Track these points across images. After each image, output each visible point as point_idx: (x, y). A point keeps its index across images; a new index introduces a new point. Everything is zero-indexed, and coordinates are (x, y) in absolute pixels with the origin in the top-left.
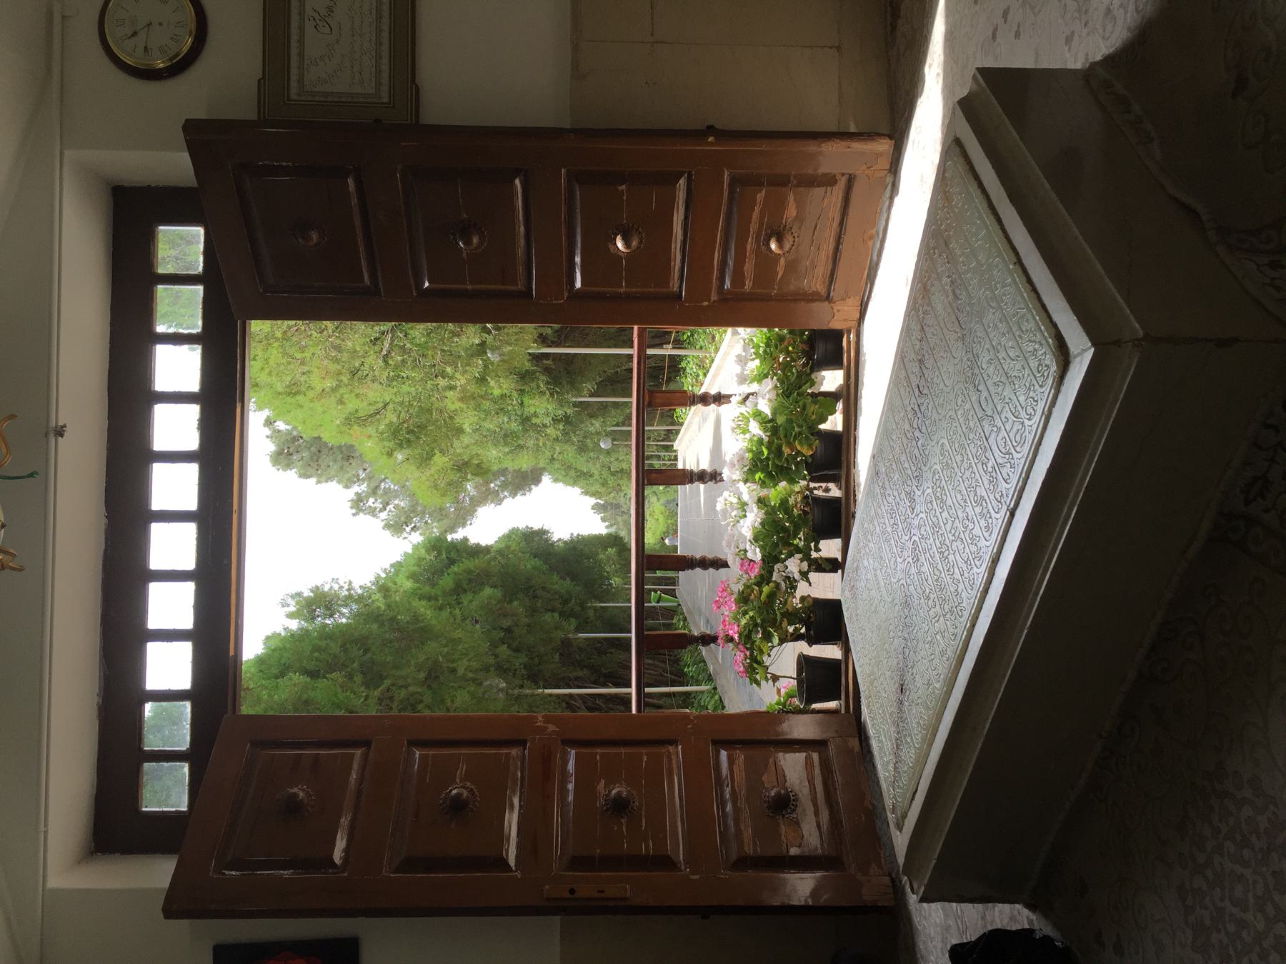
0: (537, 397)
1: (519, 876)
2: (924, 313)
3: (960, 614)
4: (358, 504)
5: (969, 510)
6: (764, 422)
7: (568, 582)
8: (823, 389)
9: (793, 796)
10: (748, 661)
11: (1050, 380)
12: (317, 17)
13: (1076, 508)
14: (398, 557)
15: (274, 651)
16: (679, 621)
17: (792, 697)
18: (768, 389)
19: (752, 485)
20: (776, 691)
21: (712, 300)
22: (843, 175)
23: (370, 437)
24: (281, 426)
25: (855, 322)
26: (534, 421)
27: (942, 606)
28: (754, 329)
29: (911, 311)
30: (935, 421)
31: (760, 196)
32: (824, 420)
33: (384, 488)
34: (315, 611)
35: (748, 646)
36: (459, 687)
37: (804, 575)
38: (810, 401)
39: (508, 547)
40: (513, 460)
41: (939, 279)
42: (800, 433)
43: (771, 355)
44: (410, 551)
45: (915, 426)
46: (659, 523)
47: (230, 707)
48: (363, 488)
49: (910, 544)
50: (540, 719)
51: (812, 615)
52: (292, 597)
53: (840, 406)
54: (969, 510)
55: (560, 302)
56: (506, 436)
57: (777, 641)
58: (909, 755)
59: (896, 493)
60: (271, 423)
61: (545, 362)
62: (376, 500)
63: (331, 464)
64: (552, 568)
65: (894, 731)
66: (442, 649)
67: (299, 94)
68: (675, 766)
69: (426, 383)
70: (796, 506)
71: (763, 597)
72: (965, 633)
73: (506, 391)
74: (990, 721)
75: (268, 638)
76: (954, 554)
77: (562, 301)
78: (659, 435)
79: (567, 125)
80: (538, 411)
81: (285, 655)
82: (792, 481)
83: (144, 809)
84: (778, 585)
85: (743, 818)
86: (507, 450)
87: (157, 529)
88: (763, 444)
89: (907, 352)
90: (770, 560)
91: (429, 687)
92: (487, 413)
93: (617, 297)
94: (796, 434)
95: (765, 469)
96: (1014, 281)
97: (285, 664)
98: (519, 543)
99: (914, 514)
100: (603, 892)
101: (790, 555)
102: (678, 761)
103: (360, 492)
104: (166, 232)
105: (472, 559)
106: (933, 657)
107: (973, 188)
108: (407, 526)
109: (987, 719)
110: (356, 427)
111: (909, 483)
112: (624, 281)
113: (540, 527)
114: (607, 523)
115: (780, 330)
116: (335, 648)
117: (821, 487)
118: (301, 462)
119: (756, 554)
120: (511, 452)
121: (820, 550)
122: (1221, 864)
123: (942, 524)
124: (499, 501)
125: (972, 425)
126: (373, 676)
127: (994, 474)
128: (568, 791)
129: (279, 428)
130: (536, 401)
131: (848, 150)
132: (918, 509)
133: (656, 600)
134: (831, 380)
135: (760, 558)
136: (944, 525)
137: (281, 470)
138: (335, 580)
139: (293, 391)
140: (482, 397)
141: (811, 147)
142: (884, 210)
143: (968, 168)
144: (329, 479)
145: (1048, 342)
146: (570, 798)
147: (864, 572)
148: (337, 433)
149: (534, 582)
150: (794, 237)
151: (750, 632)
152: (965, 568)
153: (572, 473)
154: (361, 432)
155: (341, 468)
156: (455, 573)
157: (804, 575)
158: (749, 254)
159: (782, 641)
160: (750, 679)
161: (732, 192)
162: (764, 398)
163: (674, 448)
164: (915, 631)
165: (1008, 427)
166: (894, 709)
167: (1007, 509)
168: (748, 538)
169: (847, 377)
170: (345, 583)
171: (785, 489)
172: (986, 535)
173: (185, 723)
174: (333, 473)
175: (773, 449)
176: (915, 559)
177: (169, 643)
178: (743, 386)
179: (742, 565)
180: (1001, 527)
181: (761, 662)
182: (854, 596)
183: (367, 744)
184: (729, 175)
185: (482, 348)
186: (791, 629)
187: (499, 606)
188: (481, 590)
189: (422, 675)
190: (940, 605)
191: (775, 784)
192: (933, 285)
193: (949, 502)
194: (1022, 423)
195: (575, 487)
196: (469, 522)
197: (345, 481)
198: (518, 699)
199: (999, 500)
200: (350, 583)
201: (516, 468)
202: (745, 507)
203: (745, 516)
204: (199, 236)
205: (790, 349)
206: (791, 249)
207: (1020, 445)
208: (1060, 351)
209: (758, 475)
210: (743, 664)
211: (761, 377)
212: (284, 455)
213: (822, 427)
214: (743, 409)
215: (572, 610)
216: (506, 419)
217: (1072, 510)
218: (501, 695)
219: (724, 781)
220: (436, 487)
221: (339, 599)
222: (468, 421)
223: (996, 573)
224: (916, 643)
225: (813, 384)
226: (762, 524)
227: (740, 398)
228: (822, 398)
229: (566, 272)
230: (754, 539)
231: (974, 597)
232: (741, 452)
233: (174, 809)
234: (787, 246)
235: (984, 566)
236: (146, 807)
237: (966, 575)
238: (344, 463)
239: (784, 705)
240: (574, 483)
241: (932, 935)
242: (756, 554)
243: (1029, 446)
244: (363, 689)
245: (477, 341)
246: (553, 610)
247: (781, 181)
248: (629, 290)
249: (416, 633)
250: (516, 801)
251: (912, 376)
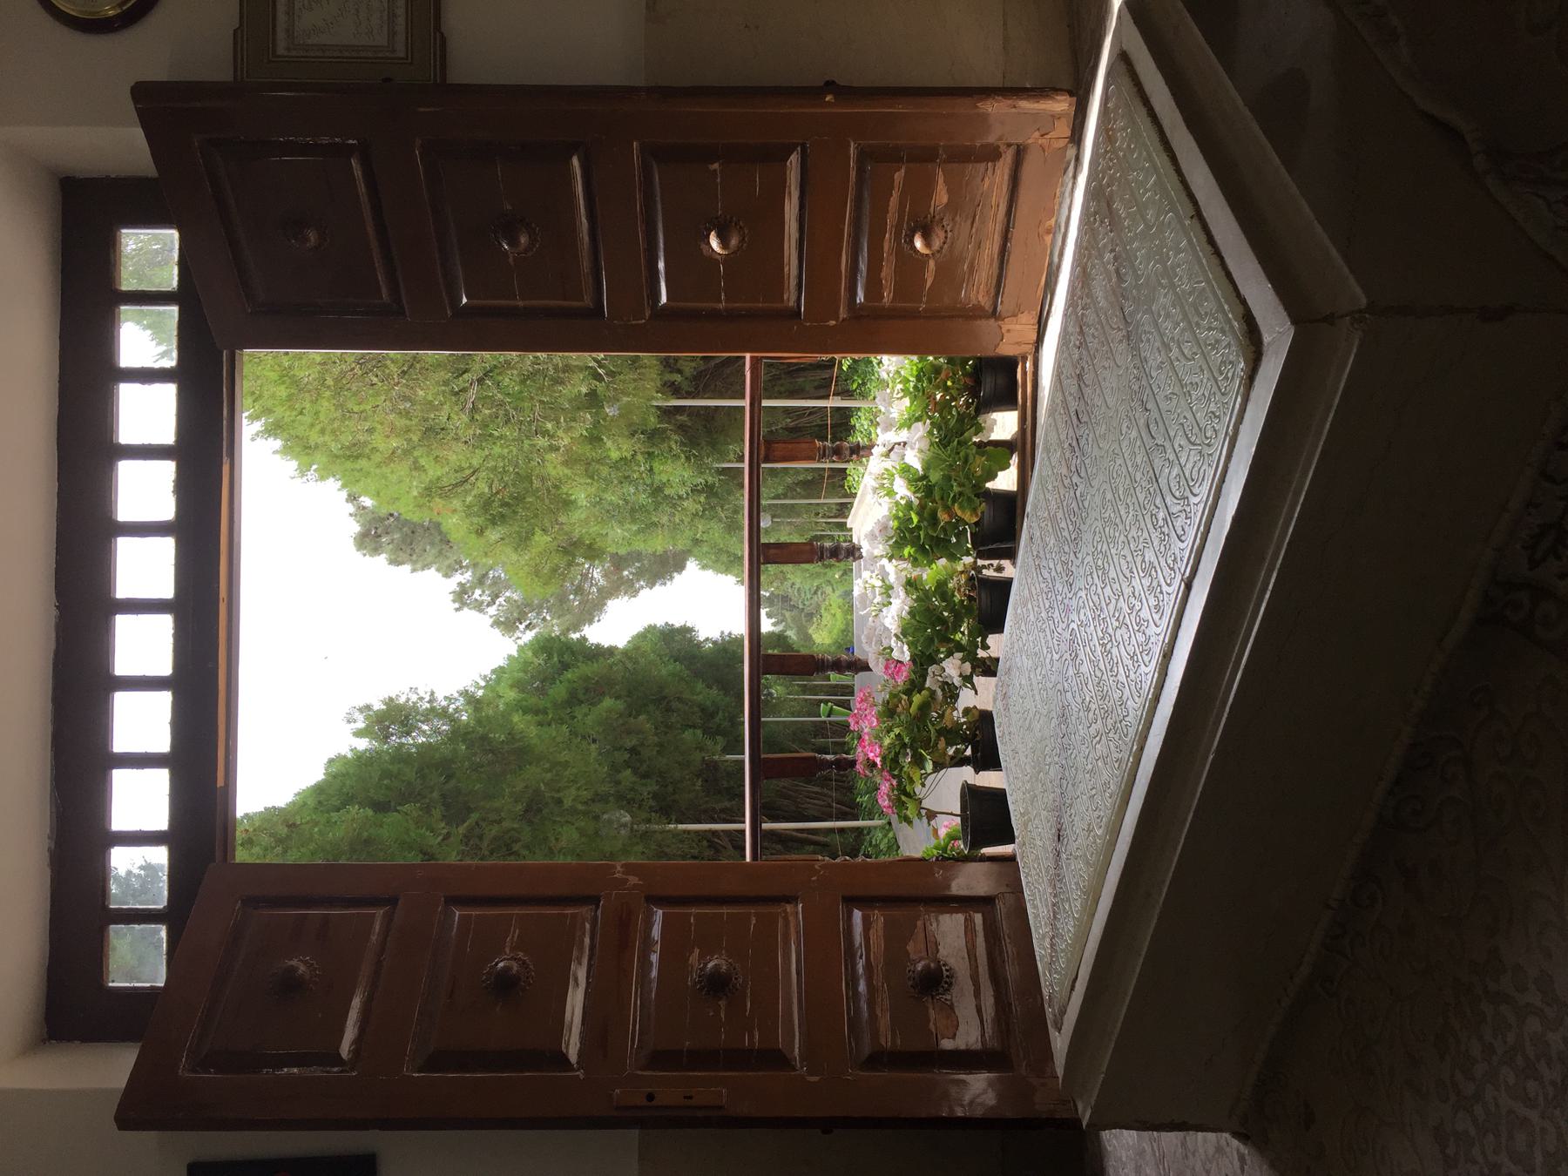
0: (670, 461)
1: (582, 1077)
2: (1083, 309)
3: (1125, 731)
4: (462, 597)
5: (1136, 582)
6: (915, 480)
7: (714, 691)
8: (994, 437)
9: (947, 970)
10: (896, 792)
13: (1275, 575)
14: (500, 661)
15: (335, 777)
16: (853, 739)
17: (956, 839)
18: (917, 436)
19: (901, 562)
20: (931, 832)
21: (841, 319)
22: (1009, 145)
23: (455, 511)
24: (367, 502)
25: (1031, 346)
26: (667, 492)
27: (1104, 721)
28: (901, 358)
29: (1069, 308)
30: (1096, 458)
31: (899, 176)
32: (993, 477)
33: (493, 577)
34: (389, 727)
35: (896, 773)
36: (567, 822)
37: (967, 679)
38: (974, 451)
39: (637, 648)
40: (644, 541)
41: (1101, 256)
42: (961, 494)
43: (924, 391)
44: (515, 654)
45: (1073, 469)
46: (836, 620)
47: (218, 854)
48: (466, 577)
49: (1067, 635)
50: (619, 868)
51: (978, 732)
52: (361, 710)
53: (1015, 460)
54: (1136, 582)
55: (640, 322)
56: (633, 510)
57: (931, 767)
58: (1068, 927)
59: (1052, 566)
60: (355, 498)
61: (679, 418)
62: (483, 592)
63: (428, 547)
64: (697, 674)
65: (1051, 894)
66: (544, 774)
67: (288, 49)
68: (792, 930)
69: (523, 442)
70: (959, 590)
71: (913, 709)
72: (1131, 760)
73: (626, 454)
74: (1167, 883)
75: (331, 761)
76: (1118, 646)
77: (644, 321)
78: (830, 509)
79: (640, 81)
80: (671, 479)
81: (348, 782)
82: (953, 558)
83: (110, 984)
84: (933, 693)
85: (880, 1000)
86: (635, 528)
87: (123, 623)
88: (912, 509)
89: (1064, 366)
90: (924, 660)
91: (530, 822)
92: (608, 482)
93: (714, 315)
94: (955, 496)
95: (915, 542)
96: (1190, 241)
97: (348, 794)
98: (656, 644)
99: (1072, 592)
100: (691, 1098)
101: (950, 654)
102: (798, 924)
103: (463, 582)
105: (589, 663)
106: (1094, 792)
108: (521, 623)
109: (1164, 881)
110: (437, 499)
111: (1066, 549)
112: (723, 294)
113: (683, 624)
114: (773, 620)
115: (935, 359)
116: (410, 774)
117: (992, 565)
118: (391, 546)
119: (903, 653)
120: (639, 531)
121: (989, 648)
122: (1495, 1098)
123: (1103, 602)
124: (634, 593)
125: (1139, 461)
126: (455, 808)
127: (1165, 530)
128: (651, 964)
129: (364, 504)
130: (669, 467)
131: (1014, 110)
133: (826, 715)
134: (1004, 424)
135: (908, 658)
136: (1107, 605)
137: (368, 556)
138: (414, 690)
139: (355, 454)
140: (598, 461)
141: (962, 106)
142: (1067, 194)
143: (1135, 90)
144: (425, 567)
145: (1232, 327)
146: (654, 973)
147: (1018, 673)
148: (414, 507)
149: (667, 691)
150: (946, 231)
151: (897, 754)
152: (1131, 667)
153: (724, 558)
154: (444, 506)
155: (440, 552)
156: (569, 681)
157: (967, 679)
158: (888, 256)
159: (938, 767)
160: (899, 816)
161: (861, 170)
162: (912, 448)
163: (848, 526)
164: (1073, 757)
166: (1051, 864)
167: (1182, 580)
168: (893, 632)
169: (1022, 420)
170: (426, 693)
171: (945, 567)
172: (1156, 617)
173: (160, 874)
174: (430, 559)
175: (925, 515)
176: (1073, 654)
177: (140, 771)
178: (889, 433)
179: (887, 668)
180: (1174, 607)
181: (912, 794)
182: (1007, 708)
183: (392, 901)
184: (857, 148)
185: (593, 400)
186: (951, 751)
187: (621, 721)
188: (600, 701)
189: (519, 808)
190: (1102, 719)
191: (924, 954)
192: (1093, 266)
193: (1112, 574)
195: (729, 575)
196: (597, 619)
197: (445, 568)
198: (645, 836)
199: (1172, 566)
200: (432, 693)
201: (650, 551)
202: (890, 592)
203: (891, 603)
204: (172, 242)
205: (949, 383)
206: (941, 248)
207: (1197, 485)
208: (1250, 339)
209: (907, 551)
210: (888, 795)
211: (908, 423)
212: (371, 537)
213: (989, 485)
214: (888, 464)
215: (719, 726)
216: (632, 490)
217: (1271, 577)
218: (623, 832)
219: (857, 952)
220: (537, 573)
221: (418, 713)
222: (581, 495)
223: (1168, 673)
224: (1074, 772)
225: (979, 429)
226: (912, 613)
227: (884, 450)
228: (992, 448)
229: (647, 282)
230: (902, 633)
231: (1142, 708)
232: (885, 520)
233: (148, 985)
234: (937, 244)
236: (113, 981)
237: (1132, 676)
238: (443, 547)
239: (944, 850)
240: (726, 570)
241: (1124, 1159)
242: (903, 652)
243: (1209, 484)
244: (443, 825)
245: (584, 390)
246: (694, 727)
247: (925, 156)
248: (731, 305)
249: (517, 754)
250: (582, 974)
251: (1070, 399)
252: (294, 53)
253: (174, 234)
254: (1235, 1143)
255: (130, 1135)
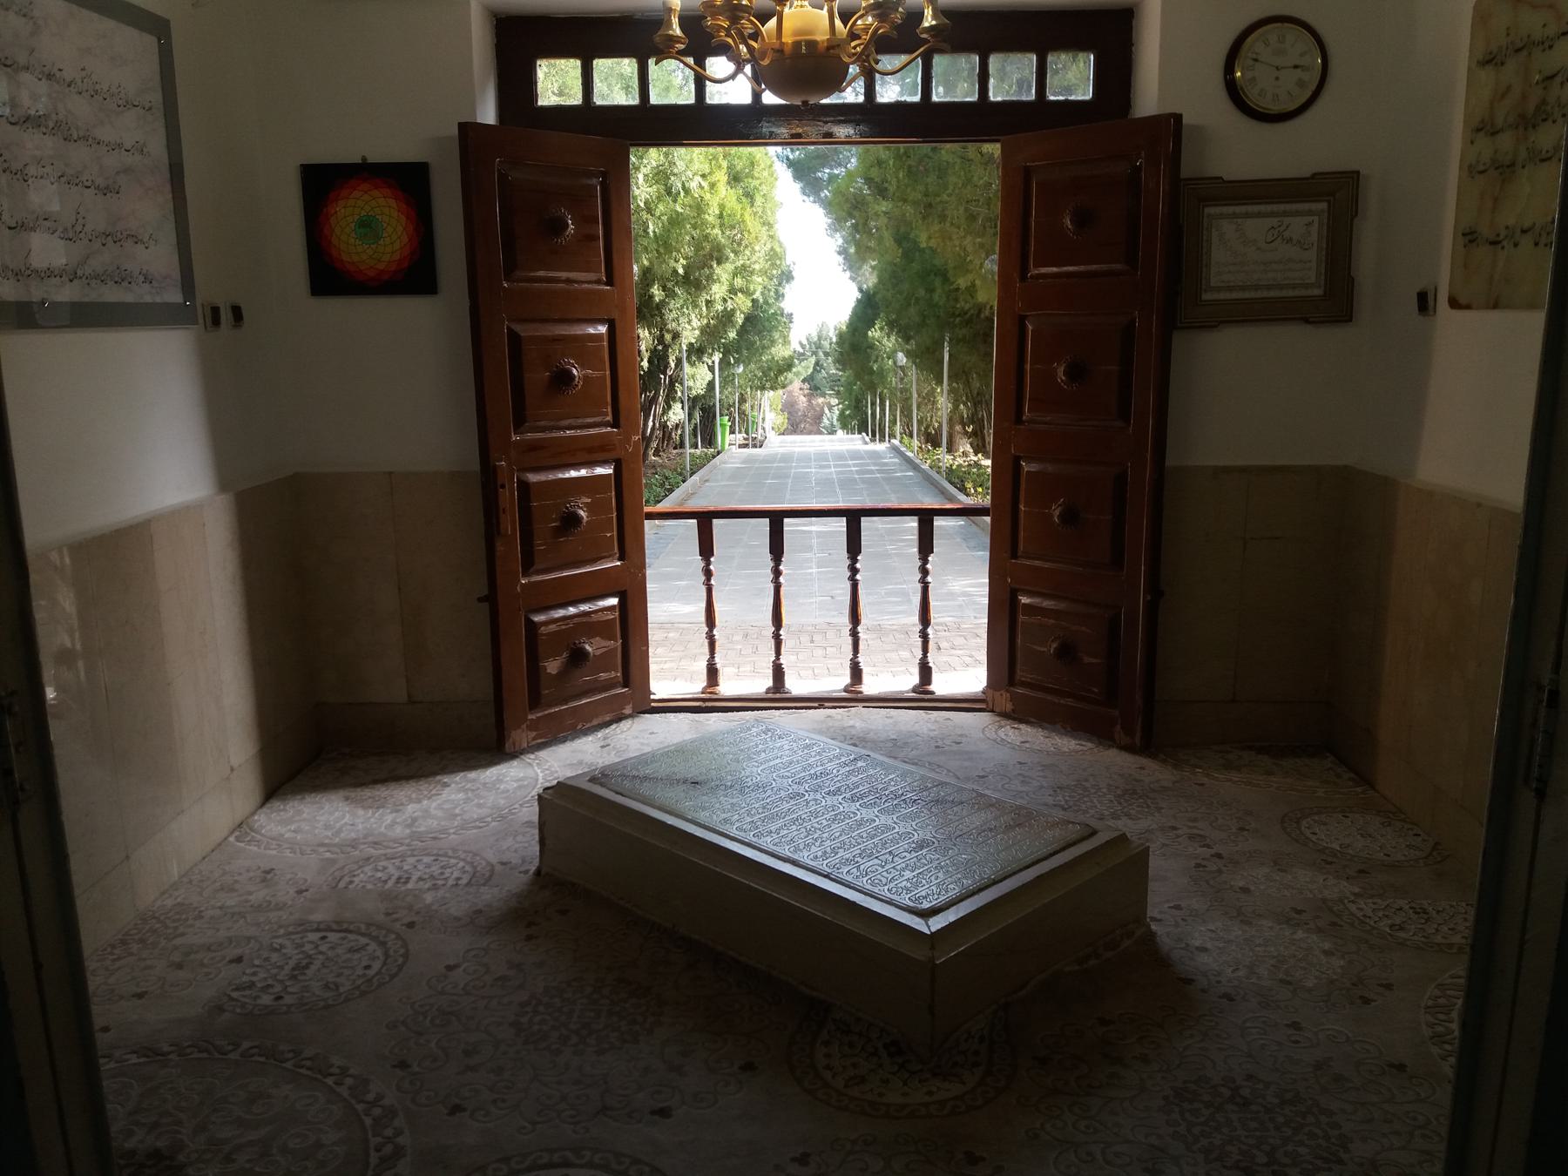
5: (828, 843)
11: (911, 904)
12: (1282, 229)
100: (504, 513)
104: (1085, 93)
107: (1055, 847)
127: (852, 862)
132: (828, 798)
152: (788, 839)
165: (884, 874)
194: (886, 885)
235: (790, 855)
237: (783, 840)
252: (1205, 219)
253: (1089, 96)
254: (534, 868)
255: (455, 131)
